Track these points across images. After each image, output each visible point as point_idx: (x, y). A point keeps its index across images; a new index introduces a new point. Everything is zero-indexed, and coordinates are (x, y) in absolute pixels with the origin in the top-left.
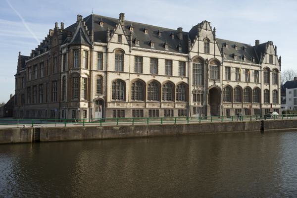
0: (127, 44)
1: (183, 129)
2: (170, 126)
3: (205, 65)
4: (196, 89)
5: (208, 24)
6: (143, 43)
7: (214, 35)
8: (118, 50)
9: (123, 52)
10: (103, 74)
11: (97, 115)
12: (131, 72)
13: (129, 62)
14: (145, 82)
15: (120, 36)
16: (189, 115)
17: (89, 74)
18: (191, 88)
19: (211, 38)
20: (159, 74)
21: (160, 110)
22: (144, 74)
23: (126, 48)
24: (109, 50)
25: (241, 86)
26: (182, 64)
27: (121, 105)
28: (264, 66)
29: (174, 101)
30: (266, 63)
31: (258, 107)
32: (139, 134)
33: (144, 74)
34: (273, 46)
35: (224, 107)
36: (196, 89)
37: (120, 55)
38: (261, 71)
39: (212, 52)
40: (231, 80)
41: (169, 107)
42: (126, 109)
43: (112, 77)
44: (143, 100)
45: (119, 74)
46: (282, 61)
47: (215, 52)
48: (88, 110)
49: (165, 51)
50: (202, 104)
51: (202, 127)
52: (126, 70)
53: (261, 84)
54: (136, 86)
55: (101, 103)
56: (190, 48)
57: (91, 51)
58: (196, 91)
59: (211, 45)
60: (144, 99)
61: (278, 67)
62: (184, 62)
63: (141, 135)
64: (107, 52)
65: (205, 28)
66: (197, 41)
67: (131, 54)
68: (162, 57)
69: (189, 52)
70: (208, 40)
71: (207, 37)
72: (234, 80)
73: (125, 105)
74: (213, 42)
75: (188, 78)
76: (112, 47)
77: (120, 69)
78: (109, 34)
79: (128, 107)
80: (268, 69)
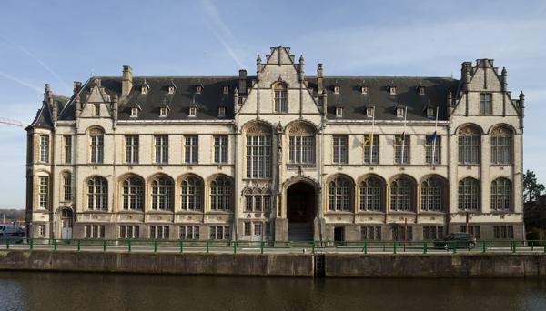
0: (318, 112)
1: (115, 262)
2: (90, 255)
3: (274, 136)
4: (251, 185)
5: (283, 51)
6: (353, 110)
7: (299, 72)
8: (500, 127)
9: (101, 130)
10: (71, 169)
11: (61, 230)
12: (117, 163)
13: (115, 147)
14: (384, 179)
15: (97, 105)
16: (234, 236)
17: (50, 170)
18: (240, 186)
19: (291, 79)
20: (141, 161)
21: (414, 228)
22: (142, 165)
23: (107, 124)
24: (80, 131)
25: (170, 174)
26: (221, 139)
27: (99, 218)
28: (456, 122)
29: (416, 211)
30: (466, 115)
31: (440, 221)
32: (37, 265)
33: (142, 165)
34: (495, 70)
35: (327, 220)
36: (251, 185)
37: (98, 134)
38: (448, 135)
39: (293, 106)
40: (350, 163)
41: (192, 221)
42: (108, 224)
43: (84, 174)
44: (350, 210)
45: (502, 169)
46: (526, 103)
47: (303, 105)
48: (48, 226)
49: (337, 119)
50: (267, 215)
51: (155, 259)
52: (108, 159)
53: (448, 166)
54: (368, 185)
55: (69, 214)
56: (451, 109)
57: (53, 136)
58: (251, 191)
59: (293, 95)
60: (414, 208)
61: (512, 121)
62: (225, 136)
63: (39, 268)
64: (76, 134)
65: (276, 61)
66: (254, 92)
67: (116, 132)
68: (388, 131)
69: (449, 116)
70: (285, 85)
71: (280, 79)
72: (422, 160)
73: (107, 217)
74: (298, 86)
75: (233, 166)
76: (83, 124)
77: (98, 158)
78: (451, 100)
79: (112, 221)
80: (477, 130)
